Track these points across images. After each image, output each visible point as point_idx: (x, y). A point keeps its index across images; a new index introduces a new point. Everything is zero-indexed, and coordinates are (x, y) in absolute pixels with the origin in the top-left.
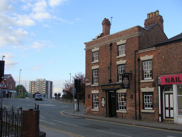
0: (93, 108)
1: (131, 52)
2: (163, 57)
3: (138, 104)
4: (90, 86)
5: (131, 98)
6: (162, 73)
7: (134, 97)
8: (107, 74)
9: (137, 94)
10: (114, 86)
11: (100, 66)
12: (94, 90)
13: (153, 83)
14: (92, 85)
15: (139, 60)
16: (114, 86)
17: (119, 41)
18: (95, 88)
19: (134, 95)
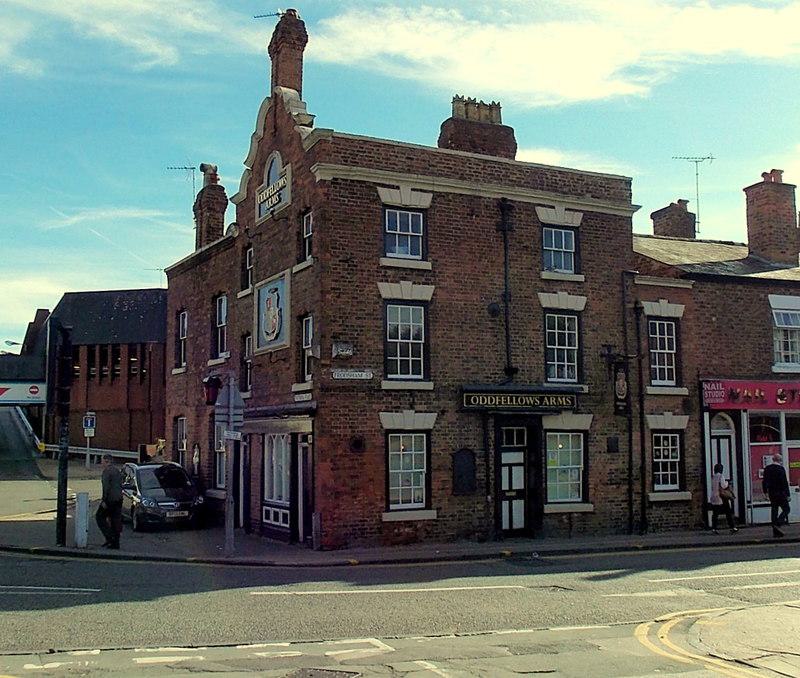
0: (388, 510)
1: (605, 272)
2: (714, 319)
3: (635, 472)
4: (372, 389)
5: (609, 451)
6: (711, 370)
7: (623, 446)
8: (488, 337)
9: (636, 436)
10: (542, 399)
11: (439, 292)
12: (397, 409)
13: (684, 401)
14: (386, 385)
15: (638, 310)
16: (542, 399)
17: (393, 187)
18: (408, 399)
19: (623, 438)
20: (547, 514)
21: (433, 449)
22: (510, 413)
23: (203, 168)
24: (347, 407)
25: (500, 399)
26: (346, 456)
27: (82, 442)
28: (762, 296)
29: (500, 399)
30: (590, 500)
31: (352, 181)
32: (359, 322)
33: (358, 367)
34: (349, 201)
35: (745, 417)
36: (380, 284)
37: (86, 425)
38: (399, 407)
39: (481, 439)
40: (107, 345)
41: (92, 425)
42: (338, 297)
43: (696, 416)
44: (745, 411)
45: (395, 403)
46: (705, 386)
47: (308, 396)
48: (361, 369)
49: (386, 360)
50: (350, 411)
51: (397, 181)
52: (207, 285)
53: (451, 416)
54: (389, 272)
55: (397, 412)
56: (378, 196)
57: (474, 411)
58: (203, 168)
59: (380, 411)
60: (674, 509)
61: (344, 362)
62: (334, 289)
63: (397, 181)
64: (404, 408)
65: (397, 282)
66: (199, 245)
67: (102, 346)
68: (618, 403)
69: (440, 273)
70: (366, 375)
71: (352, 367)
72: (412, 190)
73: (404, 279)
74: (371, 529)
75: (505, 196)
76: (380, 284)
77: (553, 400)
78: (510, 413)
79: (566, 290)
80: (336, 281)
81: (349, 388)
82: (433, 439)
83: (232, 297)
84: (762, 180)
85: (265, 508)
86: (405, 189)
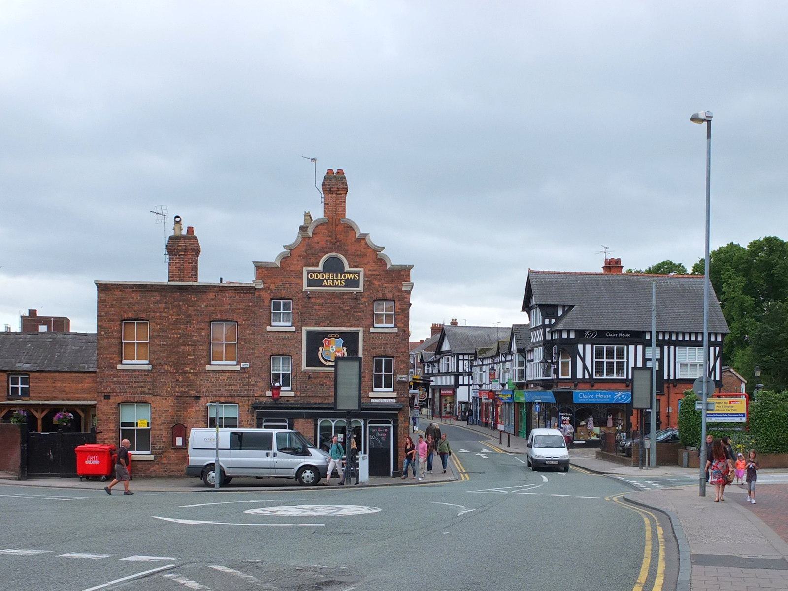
47: (395, 401)
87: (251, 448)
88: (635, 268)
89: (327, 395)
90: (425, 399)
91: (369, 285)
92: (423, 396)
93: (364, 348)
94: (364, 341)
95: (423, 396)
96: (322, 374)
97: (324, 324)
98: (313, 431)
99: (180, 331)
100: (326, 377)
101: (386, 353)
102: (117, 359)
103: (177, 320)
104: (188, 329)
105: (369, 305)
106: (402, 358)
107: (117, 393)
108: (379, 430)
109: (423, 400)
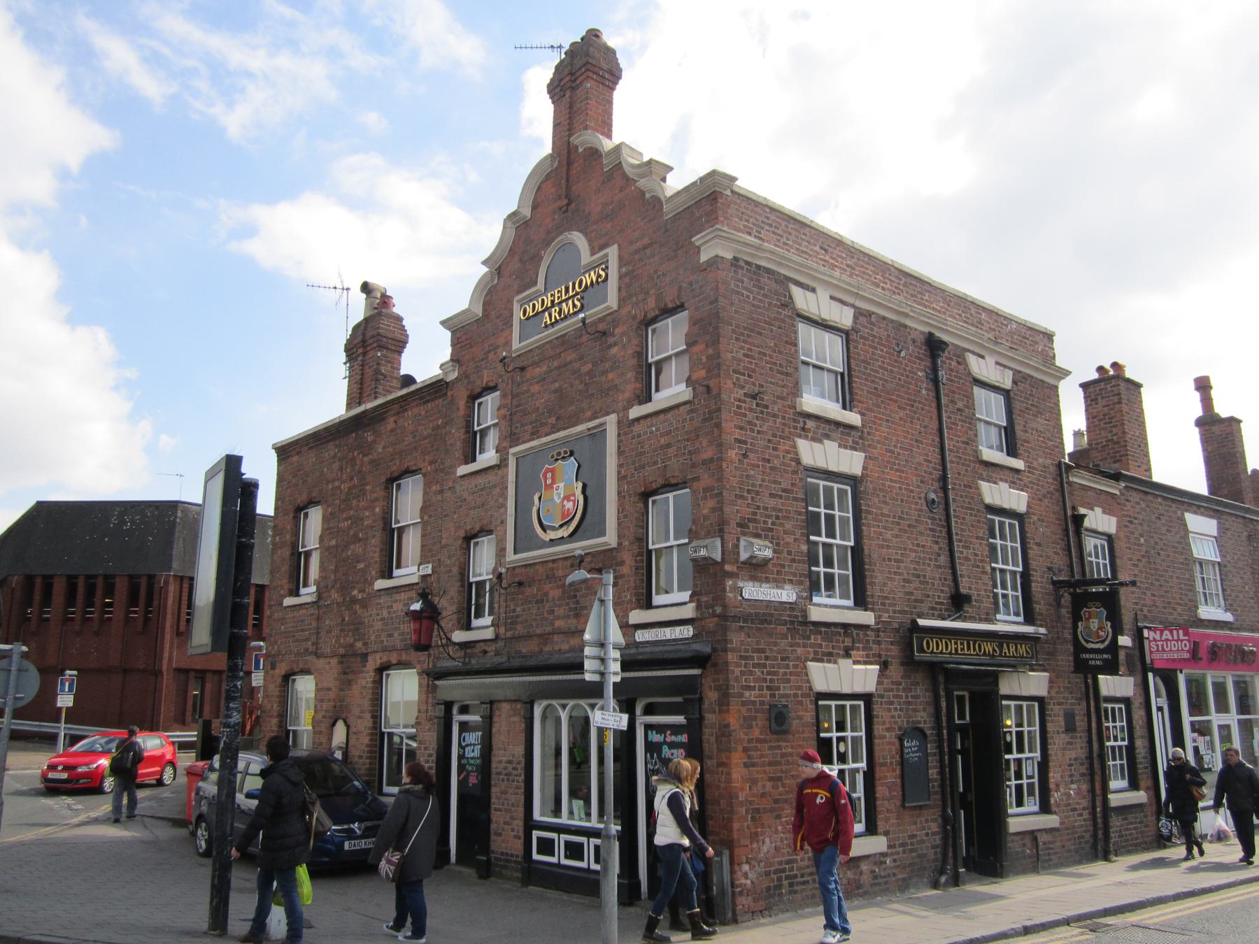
10: (1001, 647)
12: (829, 657)
15: (1078, 520)
20: (1010, 834)
21: (875, 727)
22: (972, 667)
23: (366, 288)
24: (763, 651)
25: (956, 643)
26: (765, 741)
27: (55, 716)
28: (1179, 513)
29: (956, 643)
30: (1054, 809)
31: (758, 267)
32: (772, 503)
33: (775, 581)
34: (754, 298)
35: (1181, 679)
36: (796, 439)
37: (62, 690)
38: (830, 654)
39: (931, 710)
40: (95, 577)
41: (70, 690)
42: (745, 456)
43: (1139, 677)
44: (1181, 672)
45: (826, 647)
46: (1146, 633)
47: (688, 631)
48: (779, 583)
49: (810, 571)
50: (767, 658)
51: (814, 278)
52: (372, 462)
53: (895, 671)
54: (810, 424)
55: (829, 661)
56: (791, 298)
57: (921, 663)
58: (366, 288)
59: (807, 660)
60: (1131, 817)
61: (756, 569)
62: (739, 441)
63: (814, 278)
64: (838, 655)
65: (820, 441)
66: (349, 406)
67: (88, 577)
68: (1084, 656)
69: (869, 433)
70: (787, 594)
71: (767, 580)
72: (832, 298)
73: (828, 437)
74: (802, 876)
75: (933, 331)
76: (796, 439)
77: (1012, 649)
78: (972, 667)
79: (1006, 481)
80: (741, 428)
81: (764, 616)
82: (877, 709)
83: (437, 479)
84: (1095, 376)
85: (536, 834)
86: (823, 294)
87: (571, 873)
88: (446, 353)
89: (548, 629)
90: (1107, 643)
91: (628, 286)
92: (1102, 633)
93: (619, 472)
94: (620, 452)
95: (1102, 633)
96: (540, 569)
97: (546, 429)
98: (522, 737)
99: (352, 512)
100: (548, 577)
101: (669, 475)
102: (285, 584)
103: (350, 489)
104: (361, 504)
105: (629, 341)
106: (706, 481)
107: (282, 655)
108: (671, 738)
109: (1101, 646)
